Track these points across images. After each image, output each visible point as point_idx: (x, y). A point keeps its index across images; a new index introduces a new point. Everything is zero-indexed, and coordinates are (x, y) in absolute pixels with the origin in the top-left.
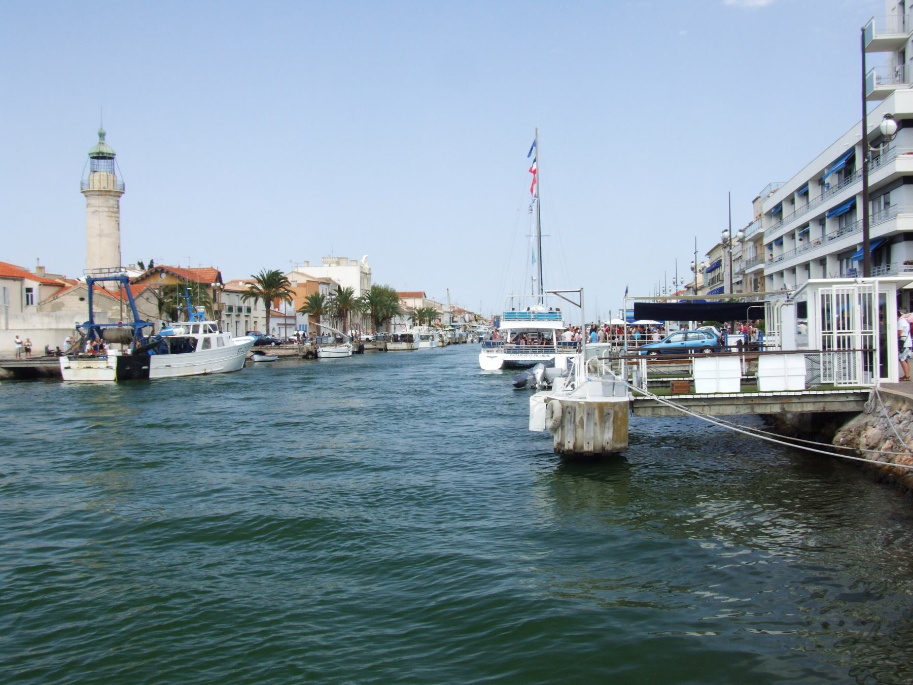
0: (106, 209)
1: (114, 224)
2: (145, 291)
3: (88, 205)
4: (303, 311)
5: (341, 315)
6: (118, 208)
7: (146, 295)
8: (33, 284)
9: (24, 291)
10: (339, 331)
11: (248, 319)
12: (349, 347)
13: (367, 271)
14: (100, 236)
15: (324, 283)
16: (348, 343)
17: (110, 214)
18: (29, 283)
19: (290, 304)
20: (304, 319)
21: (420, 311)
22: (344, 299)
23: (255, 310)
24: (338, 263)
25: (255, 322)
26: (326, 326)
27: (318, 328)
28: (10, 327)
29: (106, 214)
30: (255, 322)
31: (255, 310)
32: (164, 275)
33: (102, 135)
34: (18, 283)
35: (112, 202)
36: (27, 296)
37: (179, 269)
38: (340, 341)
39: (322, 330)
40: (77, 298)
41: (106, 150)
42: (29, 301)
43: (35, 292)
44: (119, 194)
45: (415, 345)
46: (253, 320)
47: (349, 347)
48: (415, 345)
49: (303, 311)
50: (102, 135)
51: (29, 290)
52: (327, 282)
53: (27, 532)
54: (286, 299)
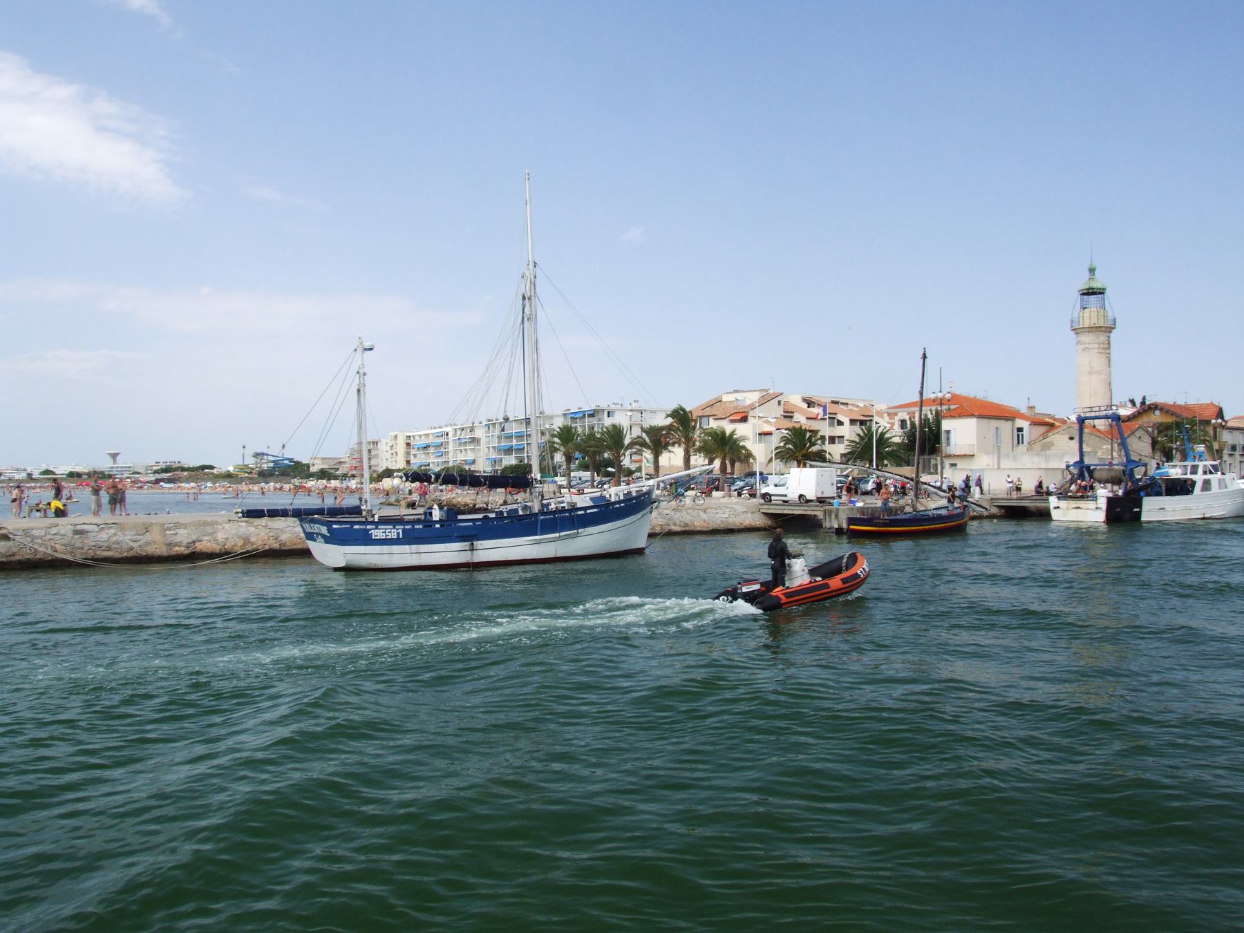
3: (1078, 343)
14: (1090, 373)
18: (1020, 423)
33: (1092, 271)
37: (1174, 405)
41: (1096, 285)
42: (1020, 440)
43: (1025, 432)
44: (1109, 330)
50: (1092, 271)
51: (1020, 430)
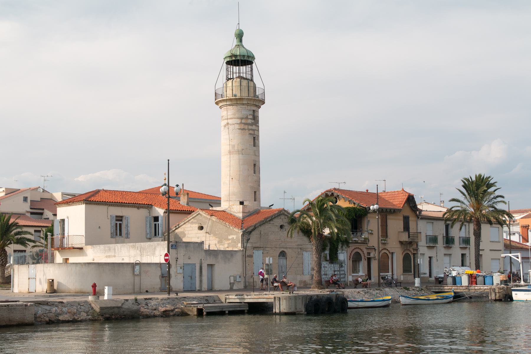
17: (242, 126)
34: (143, 212)
36: (155, 225)
51: (156, 219)
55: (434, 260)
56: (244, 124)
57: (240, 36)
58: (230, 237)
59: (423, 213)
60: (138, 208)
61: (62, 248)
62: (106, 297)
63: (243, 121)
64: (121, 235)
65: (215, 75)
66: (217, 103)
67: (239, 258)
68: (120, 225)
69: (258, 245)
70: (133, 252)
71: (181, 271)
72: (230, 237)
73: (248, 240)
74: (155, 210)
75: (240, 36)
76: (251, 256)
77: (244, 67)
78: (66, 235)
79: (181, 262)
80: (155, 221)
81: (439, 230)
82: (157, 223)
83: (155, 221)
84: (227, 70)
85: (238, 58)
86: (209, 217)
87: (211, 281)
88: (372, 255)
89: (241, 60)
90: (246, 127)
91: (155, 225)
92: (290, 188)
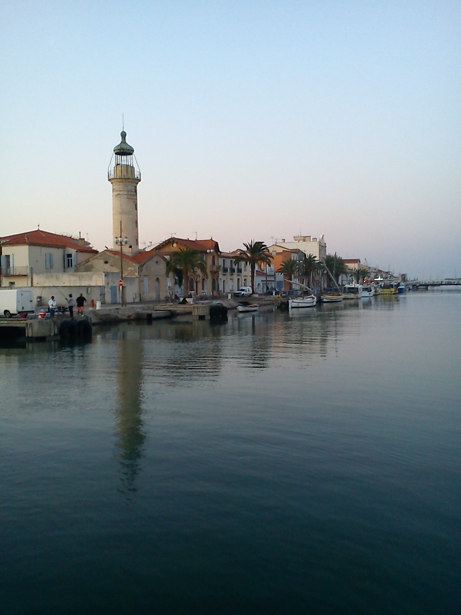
0: (126, 193)
1: (411, 297)
2: (155, 256)
4: (280, 271)
5: (306, 274)
6: (136, 191)
7: (155, 259)
8: (72, 251)
9: (66, 256)
10: (304, 286)
11: (239, 277)
12: (313, 298)
13: (323, 245)
15: (295, 253)
16: (313, 296)
17: (129, 197)
19: (270, 266)
20: (280, 277)
21: (358, 271)
22: (309, 261)
23: (245, 270)
24: (304, 241)
25: (245, 280)
26: (296, 284)
27: (291, 284)
28: (34, 285)
29: (126, 196)
30: (245, 280)
31: (245, 270)
32: (175, 245)
34: (61, 251)
35: (131, 187)
36: (69, 260)
38: (306, 293)
39: (294, 286)
40: (102, 262)
45: (359, 295)
46: (243, 278)
47: (313, 298)
48: (359, 295)
49: (280, 271)
51: (70, 256)
52: (297, 251)
53: (260, 366)
54: (266, 262)
55: (225, 282)
56: (130, 195)
57: (124, 135)
58: (130, 269)
59: (222, 254)
60: (58, 248)
61: (8, 276)
62: (98, 308)
63: (129, 193)
64: (71, 266)
65: (108, 162)
66: (109, 180)
67: (137, 281)
68: (71, 260)
69: (146, 274)
70: (72, 278)
71: (110, 291)
72: (130, 269)
73: (141, 271)
74: (60, 249)
75: (124, 135)
76: (143, 281)
77: (125, 156)
78: (11, 266)
79: (110, 285)
80: (68, 257)
81: (228, 265)
82: (70, 258)
83: (68, 257)
84: (117, 159)
85: (125, 151)
86: (113, 256)
87: (123, 297)
88: (198, 280)
89: (124, 151)
90: (131, 197)
91: (69, 260)
92: (149, 237)
